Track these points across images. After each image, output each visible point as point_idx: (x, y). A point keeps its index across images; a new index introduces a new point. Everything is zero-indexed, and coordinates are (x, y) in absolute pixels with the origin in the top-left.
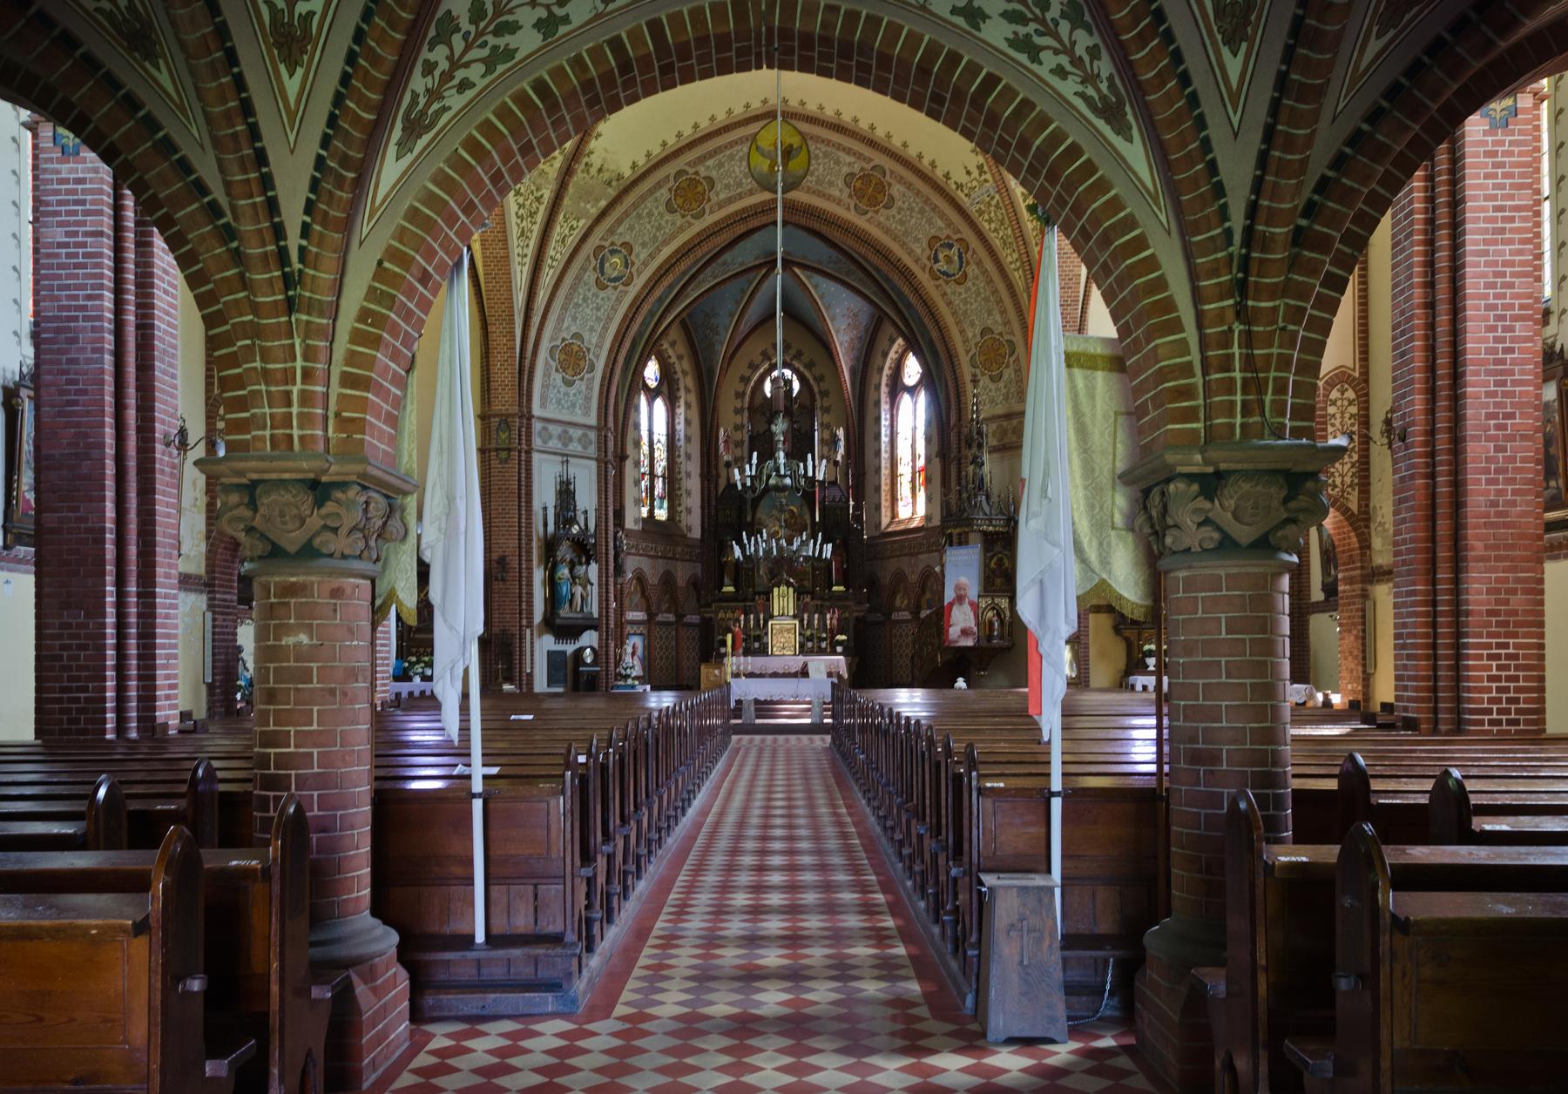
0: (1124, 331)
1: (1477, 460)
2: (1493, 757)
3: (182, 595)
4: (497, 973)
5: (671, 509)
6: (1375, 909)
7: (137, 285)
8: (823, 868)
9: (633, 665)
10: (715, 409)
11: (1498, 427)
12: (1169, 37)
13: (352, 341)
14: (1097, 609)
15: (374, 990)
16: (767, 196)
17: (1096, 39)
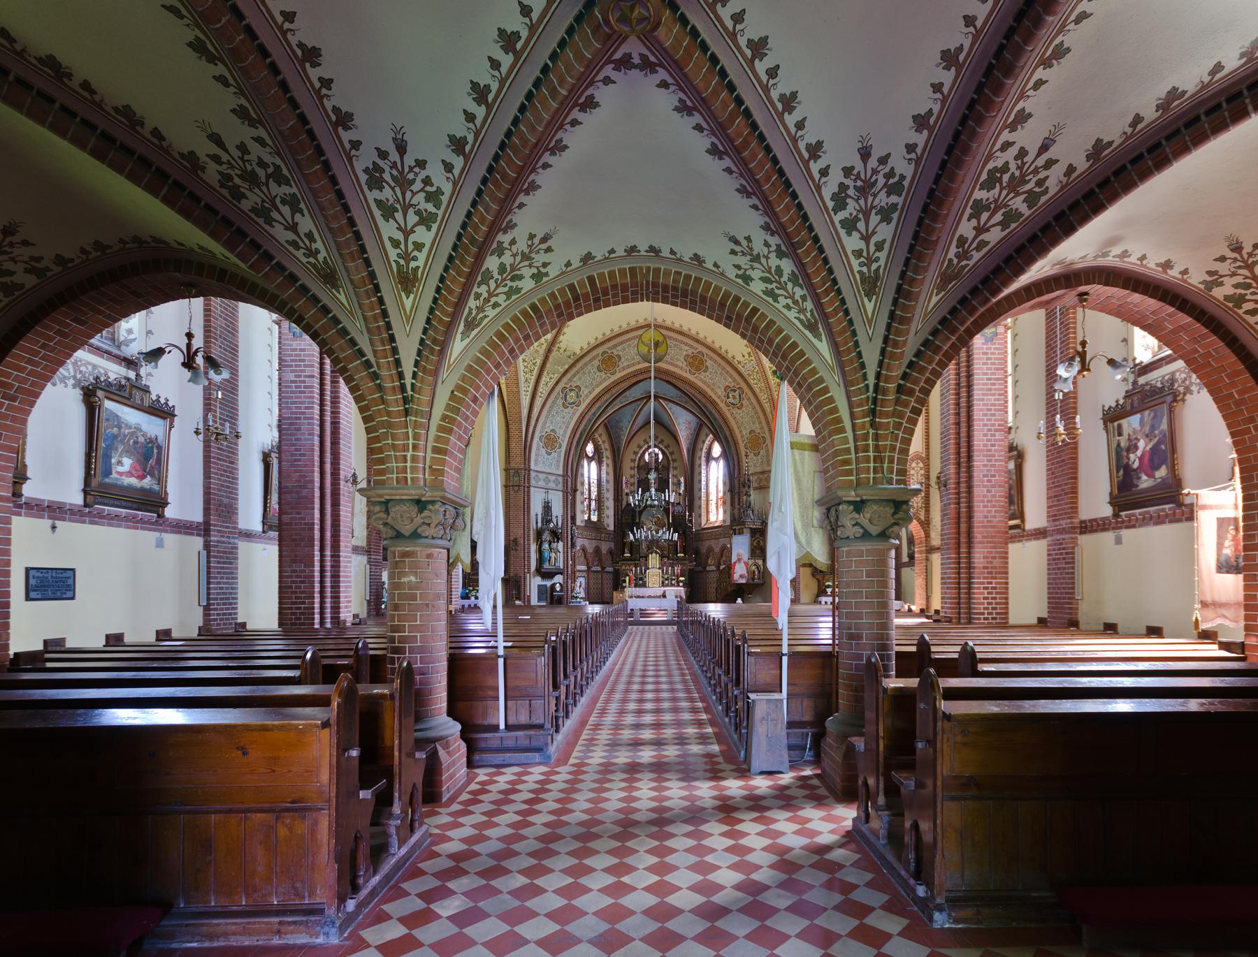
0: (818, 432)
1: (978, 496)
2: (984, 635)
3: (354, 556)
4: (511, 743)
5: (599, 516)
6: (935, 709)
7: (332, 402)
8: (672, 690)
9: (580, 591)
10: (621, 468)
11: (988, 481)
12: (839, 292)
13: (438, 431)
14: (804, 565)
15: (448, 753)
16: (647, 364)
17: (805, 292)
